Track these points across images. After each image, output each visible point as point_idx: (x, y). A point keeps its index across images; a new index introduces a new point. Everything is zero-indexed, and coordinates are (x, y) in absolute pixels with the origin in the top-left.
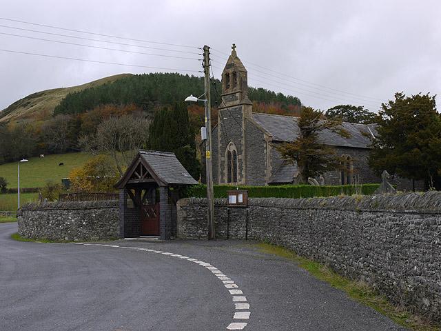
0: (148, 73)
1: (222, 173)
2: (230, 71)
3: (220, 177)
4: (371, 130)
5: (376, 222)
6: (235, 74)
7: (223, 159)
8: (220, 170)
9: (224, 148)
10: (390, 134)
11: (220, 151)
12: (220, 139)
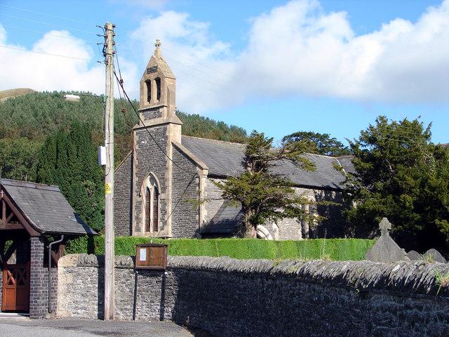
0: (51, 90)
2: (152, 77)
4: (347, 162)
5: (402, 317)
6: (158, 81)
9: (140, 184)
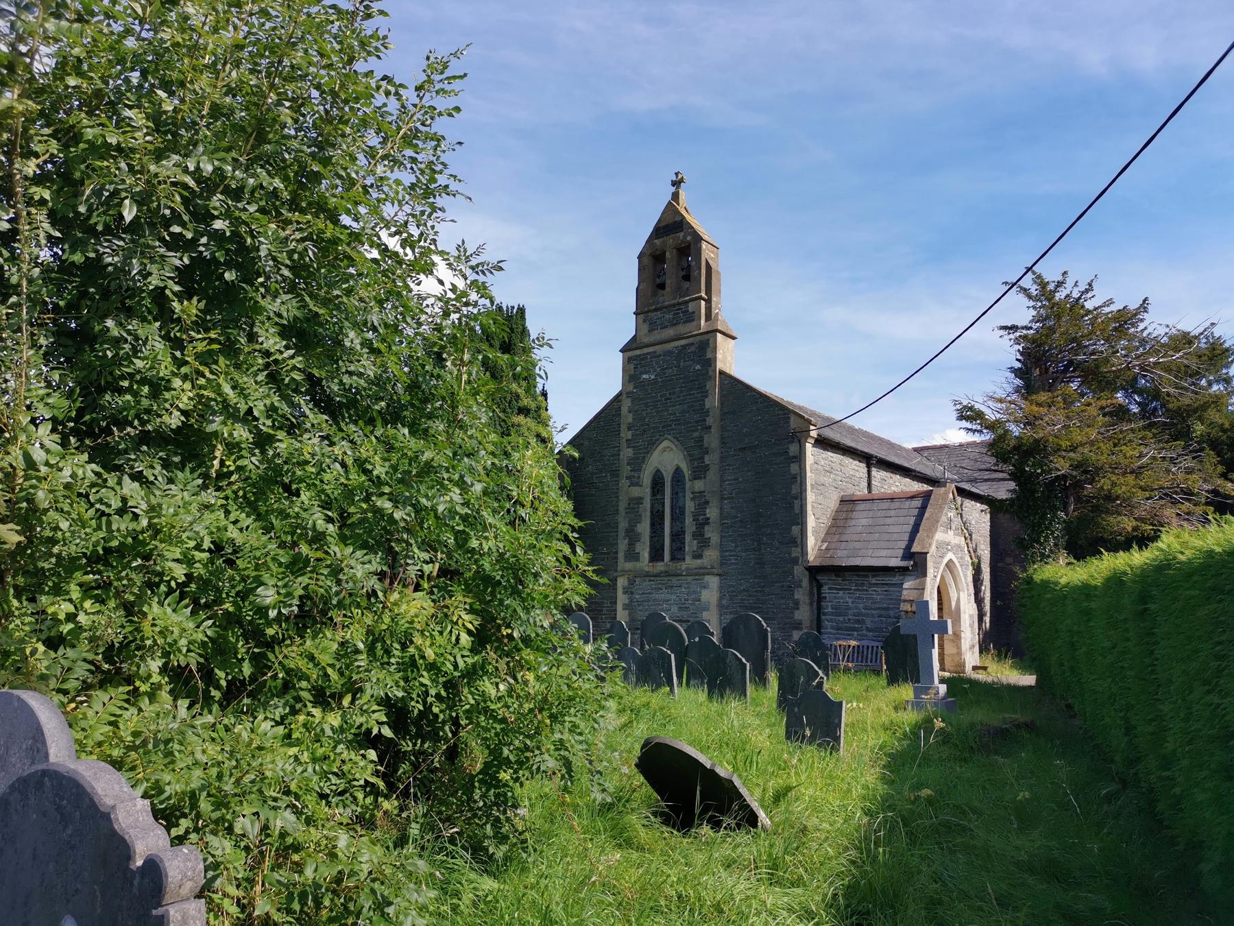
1: (633, 536)
3: (623, 545)
7: (636, 492)
8: (623, 525)
10: (1108, 512)
11: (626, 470)
12: (626, 435)
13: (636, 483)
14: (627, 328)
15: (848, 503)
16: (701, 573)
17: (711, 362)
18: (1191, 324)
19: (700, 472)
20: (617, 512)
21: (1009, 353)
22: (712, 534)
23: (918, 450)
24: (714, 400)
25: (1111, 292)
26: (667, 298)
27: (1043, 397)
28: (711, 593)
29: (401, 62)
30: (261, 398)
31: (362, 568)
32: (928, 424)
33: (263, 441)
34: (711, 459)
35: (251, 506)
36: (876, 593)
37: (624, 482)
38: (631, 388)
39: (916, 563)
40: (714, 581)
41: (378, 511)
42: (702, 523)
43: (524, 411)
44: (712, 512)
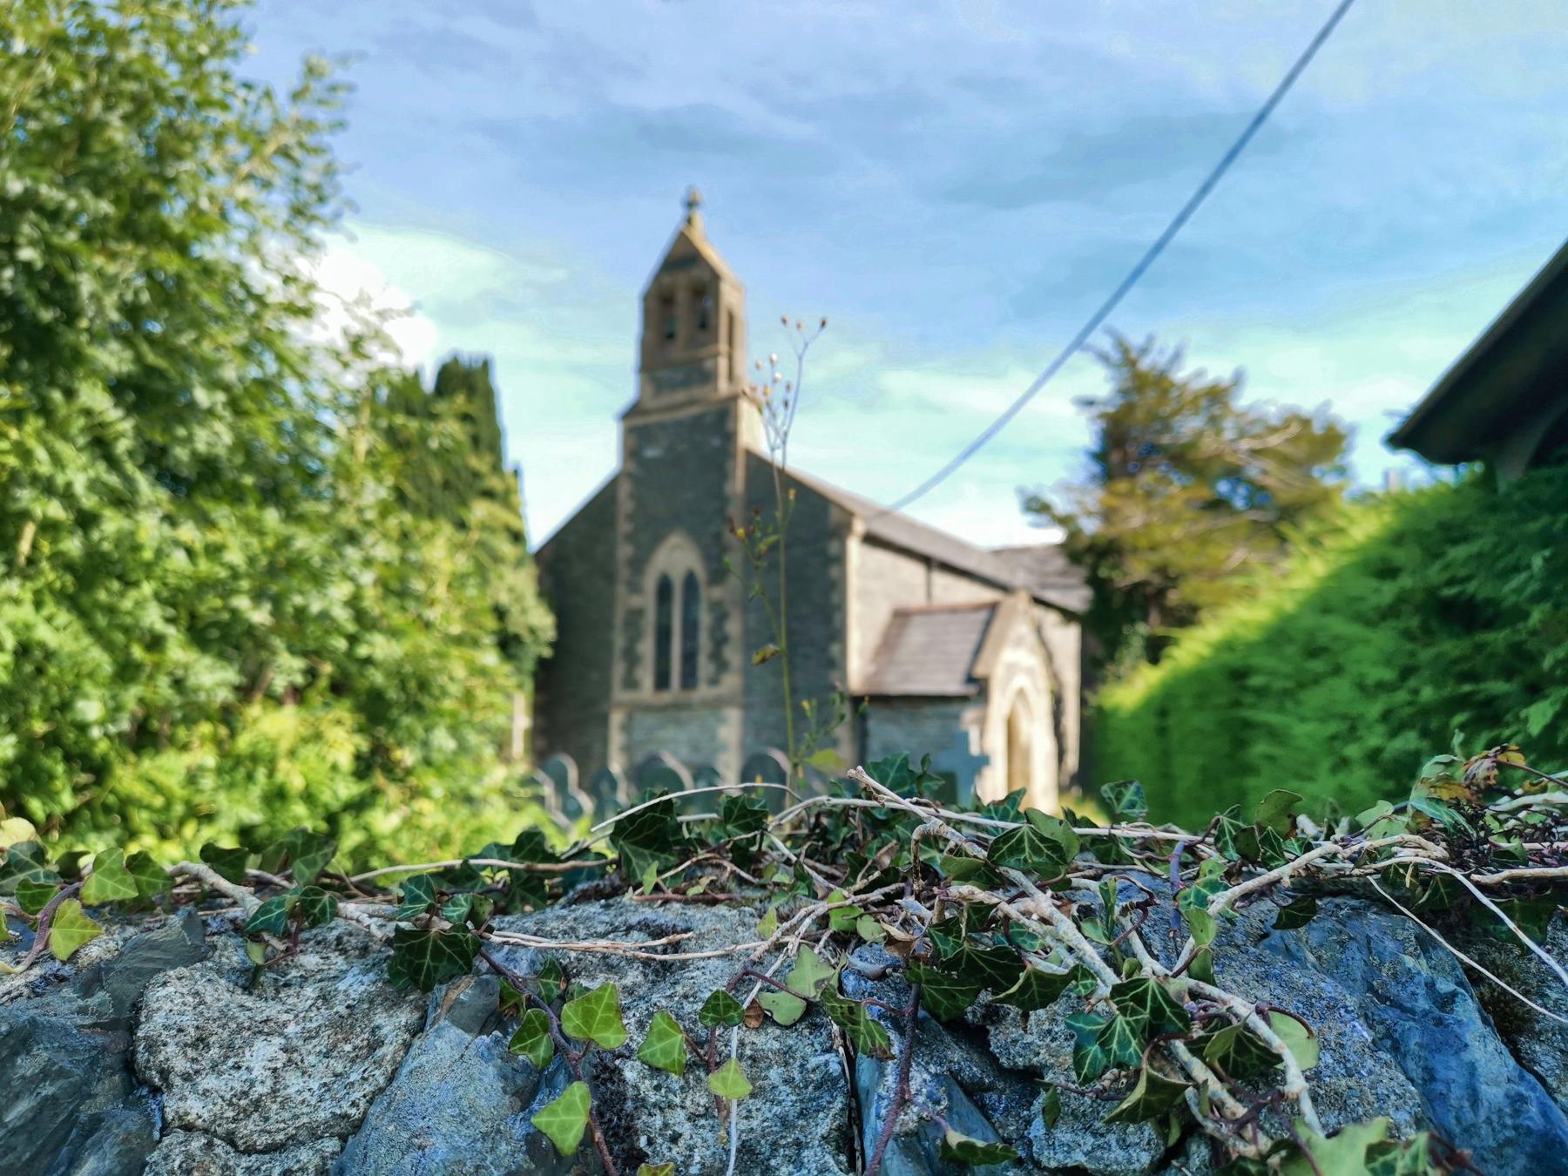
1: (632, 659)
3: (618, 670)
7: (635, 601)
8: (619, 641)
11: (624, 573)
12: (624, 527)
13: (635, 588)
14: (627, 389)
15: (902, 617)
16: (716, 705)
17: (730, 437)
18: (1307, 404)
19: (718, 575)
20: (609, 626)
21: (1084, 434)
22: (733, 655)
23: (998, 553)
24: (737, 483)
25: (1201, 366)
26: (677, 352)
27: (1122, 486)
28: (731, 729)
29: (266, 61)
30: (79, 473)
31: (213, 678)
32: (989, 518)
33: (85, 521)
34: (733, 560)
35: (71, 601)
36: (931, 726)
37: (621, 590)
38: (632, 467)
39: (979, 689)
40: (734, 715)
41: (234, 612)
42: (720, 641)
43: (489, 494)
44: (733, 627)
